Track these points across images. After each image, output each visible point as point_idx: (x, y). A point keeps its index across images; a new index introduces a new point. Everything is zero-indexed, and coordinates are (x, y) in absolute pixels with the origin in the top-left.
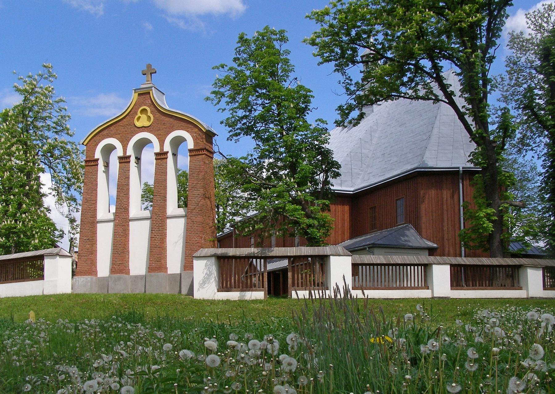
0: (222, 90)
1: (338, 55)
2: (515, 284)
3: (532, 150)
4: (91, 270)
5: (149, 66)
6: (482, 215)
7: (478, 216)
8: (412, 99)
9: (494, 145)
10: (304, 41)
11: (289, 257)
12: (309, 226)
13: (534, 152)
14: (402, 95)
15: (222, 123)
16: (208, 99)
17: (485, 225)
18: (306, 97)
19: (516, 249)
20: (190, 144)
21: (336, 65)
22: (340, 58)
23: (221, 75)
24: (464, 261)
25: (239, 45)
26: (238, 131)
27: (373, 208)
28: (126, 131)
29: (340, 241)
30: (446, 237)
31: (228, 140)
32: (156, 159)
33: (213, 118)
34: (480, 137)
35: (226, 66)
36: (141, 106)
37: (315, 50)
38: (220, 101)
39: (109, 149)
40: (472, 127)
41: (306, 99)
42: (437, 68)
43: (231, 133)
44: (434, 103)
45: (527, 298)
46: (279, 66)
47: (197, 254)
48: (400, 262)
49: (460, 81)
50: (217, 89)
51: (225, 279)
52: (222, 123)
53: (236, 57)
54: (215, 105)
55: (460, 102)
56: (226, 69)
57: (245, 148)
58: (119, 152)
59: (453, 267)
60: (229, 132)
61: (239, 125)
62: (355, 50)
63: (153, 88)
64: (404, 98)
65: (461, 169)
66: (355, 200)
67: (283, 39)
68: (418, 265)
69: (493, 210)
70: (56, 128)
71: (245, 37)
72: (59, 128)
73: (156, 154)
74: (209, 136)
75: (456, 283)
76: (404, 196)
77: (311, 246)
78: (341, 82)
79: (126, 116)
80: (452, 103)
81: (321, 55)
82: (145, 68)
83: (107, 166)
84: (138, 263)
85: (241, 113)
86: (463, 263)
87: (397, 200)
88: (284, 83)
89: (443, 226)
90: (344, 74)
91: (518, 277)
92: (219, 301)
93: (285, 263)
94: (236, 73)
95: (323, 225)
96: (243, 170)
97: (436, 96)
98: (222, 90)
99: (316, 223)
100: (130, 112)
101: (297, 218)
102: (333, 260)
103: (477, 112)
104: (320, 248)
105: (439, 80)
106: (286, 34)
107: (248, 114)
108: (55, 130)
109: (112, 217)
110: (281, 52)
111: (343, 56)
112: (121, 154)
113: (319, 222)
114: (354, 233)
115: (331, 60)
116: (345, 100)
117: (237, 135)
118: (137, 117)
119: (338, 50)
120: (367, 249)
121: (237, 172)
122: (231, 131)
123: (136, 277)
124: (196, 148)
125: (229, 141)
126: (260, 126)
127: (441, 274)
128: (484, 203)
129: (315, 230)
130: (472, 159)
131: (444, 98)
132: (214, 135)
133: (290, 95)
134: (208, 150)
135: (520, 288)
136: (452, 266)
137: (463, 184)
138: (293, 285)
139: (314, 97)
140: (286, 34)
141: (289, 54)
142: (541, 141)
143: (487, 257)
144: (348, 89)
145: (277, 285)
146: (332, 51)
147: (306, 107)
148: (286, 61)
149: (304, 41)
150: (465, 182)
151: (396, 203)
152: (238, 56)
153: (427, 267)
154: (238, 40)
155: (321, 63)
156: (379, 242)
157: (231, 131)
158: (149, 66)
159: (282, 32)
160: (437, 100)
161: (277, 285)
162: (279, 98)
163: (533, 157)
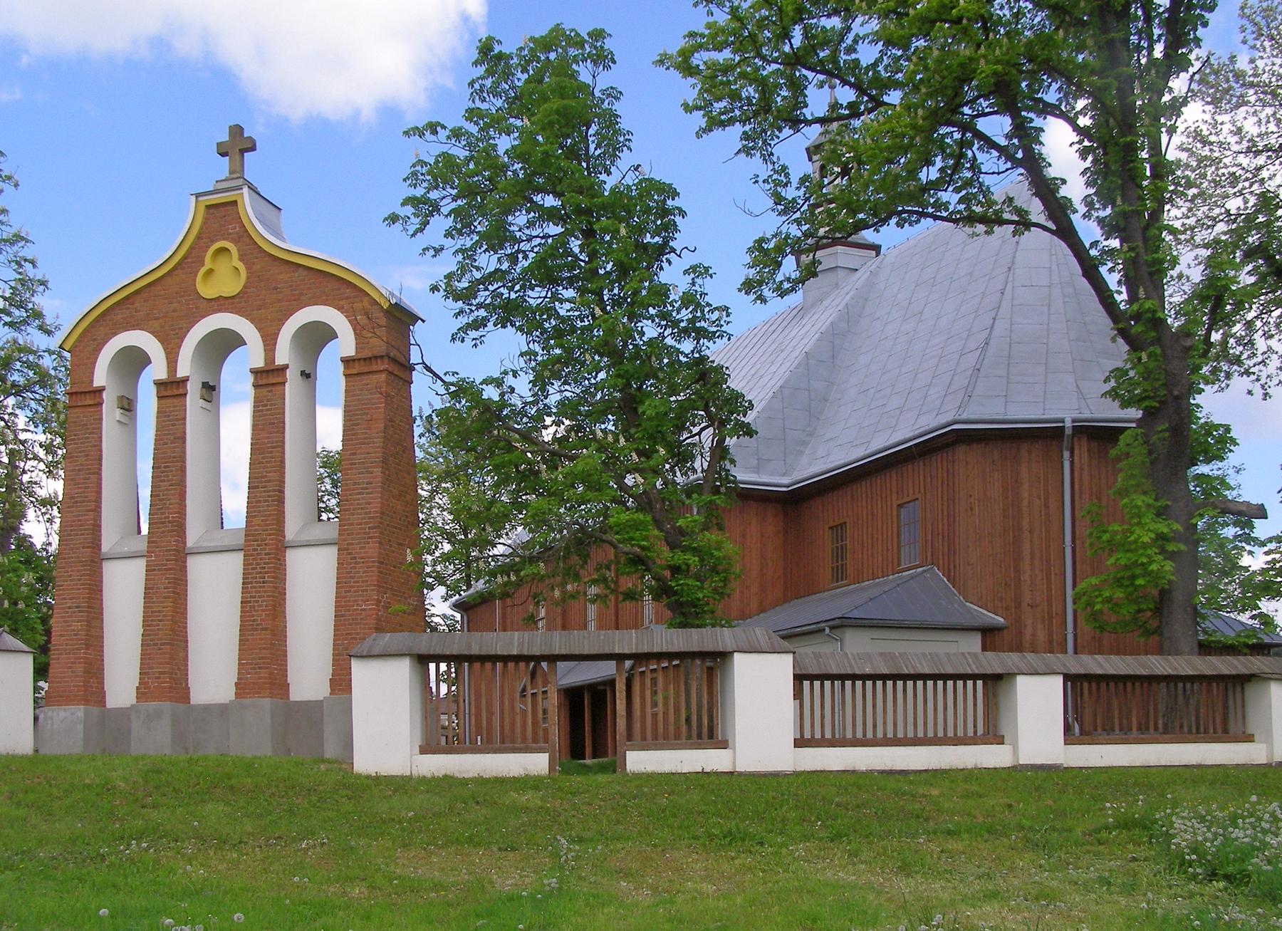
0: (434, 195)
1: (750, 104)
2: (1225, 728)
3: (1247, 373)
4: (93, 690)
5: (237, 131)
6: (1146, 539)
7: (1135, 541)
8: (956, 221)
9: (1188, 343)
10: (661, 62)
11: (619, 658)
12: (676, 570)
13: (1253, 377)
14: (930, 210)
15: (434, 289)
16: (393, 219)
17: (1154, 567)
18: (665, 212)
19: (1233, 634)
20: (345, 343)
21: (746, 137)
22: (756, 114)
23: (431, 149)
24: (1101, 666)
25: (481, 70)
26: (482, 313)
27: (838, 529)
28: (175, 311)
29: (754, 605)
30: (1027, 598)
31: (453, 339)
32: (256, 386)
33: (410, 271)
34: (1139, 327)
35: (444, 127)
36: (213, 242)
37: (689, 89)
38: (425, 224)
39: (134, 361)
40: (1118, 298)
41: (666, 220)
42: (1026, 135)
43: (463, 320)
44: (1014, 233)
45: (1268, 765)
46: (591, 132)
47: (364, 648)
48: (927, 671)
49: (1083, 173)
50: (419, 192)
51: (483, 691)
52: (434, 289)
53: (472, 105)
54: (413, 236)
55: (1089, 231)
56: (443, 134)
57: (498, 359)
58: (157, 370)
59: (1074, 682)
60: (457, 315)
61: (483, 296)
62: (798, 87)
63: (246, 190)
64: (936, 218)
65: (1068, 424)
66: (794, 503)
67: (603, 59)
68: (974, 677)
69: (1176, 526)
70: (9, 314)
71: (497, 49)
72: (17, 313)
73: (255, 372)
74: (401, 319)
75: (1079, 727)
76: (918, 496)
77: (683, 625)
78: (760, 179)
79: (174, 269)
80: (1066, 232)
81: (705, 107)
82: (225, 137)
83: (128, 406)
84: (213, 671)
85: (488, 262)
86: (1099, 671)
87: (900, 506)
88: (603, 177)
89: (1017, 570)
90: (768, 157)
91: (1243, 706)
92: (423, 780)
93: (606, 670)
94: (469, 144)
95: (715, 568)
96: (491, 414)
97: (1022, 213)
98: (434, 195)
99: (693, 560)
100: (185, 257)
101: (639, 546)
102: (741, 662)
103: (1142, 251)
104: (707, 632)
105: (1033, 165)
106: (608, 44)
107: (505, 266)
108: (8, 319)
109: (142, 546)
110: (597, 94)
111: (766, 106)
112: (163, 375)
113: (702, 560)
114: (796, 586)
115: (731, 121)
116: (771, 224)
117: (478, 324)
118: (203, 271)
119: (750, 91)
120: (827, 630)
121: (480, 424)
122: (461, 312)
123: (207, 708)
124: (367, 354)
125: (458, 342)
126: (536, 296)
127: (1038, 704)
128: (1148, 506)
129: (690, 582)
130: (1113, 389)
131: (1042, 219)
132: (415, 318)
133: (621, 205)
134: (395, 361)
135: (1249, 738)
136: (1067, 677)
137: (1072, 463)
138: (630, 737)
139: (683, 213)
140: (608, 44)
141: (617, 99)
142: (1270, 349)
143: (1157, 655)
144: (778, 199)
145: (589, 724)
146: (735, 96)
147: (666, 243)
148: (611, 120)
149: (661, 62)
150: (1076, 452)
151: (898, 516)
152: (478, 104)
153: (996, 682)
154: (475, 55)
155: (708, 130)
156: (856, 614)
157: (461, 312)
158: (237, 131)
159: (598, 35)
160: (1024, 223)
161: (589, 724)
162: (587, 212)
163: (1250, 392)
